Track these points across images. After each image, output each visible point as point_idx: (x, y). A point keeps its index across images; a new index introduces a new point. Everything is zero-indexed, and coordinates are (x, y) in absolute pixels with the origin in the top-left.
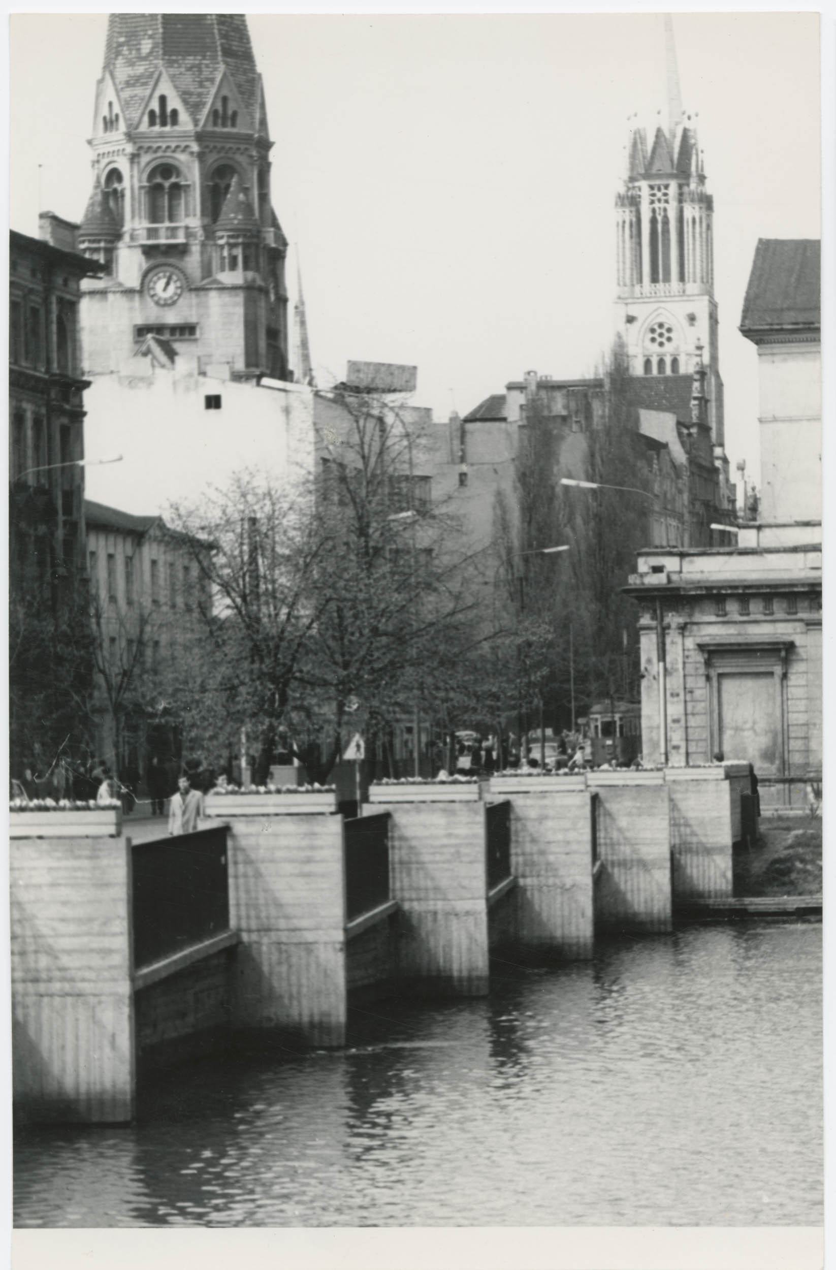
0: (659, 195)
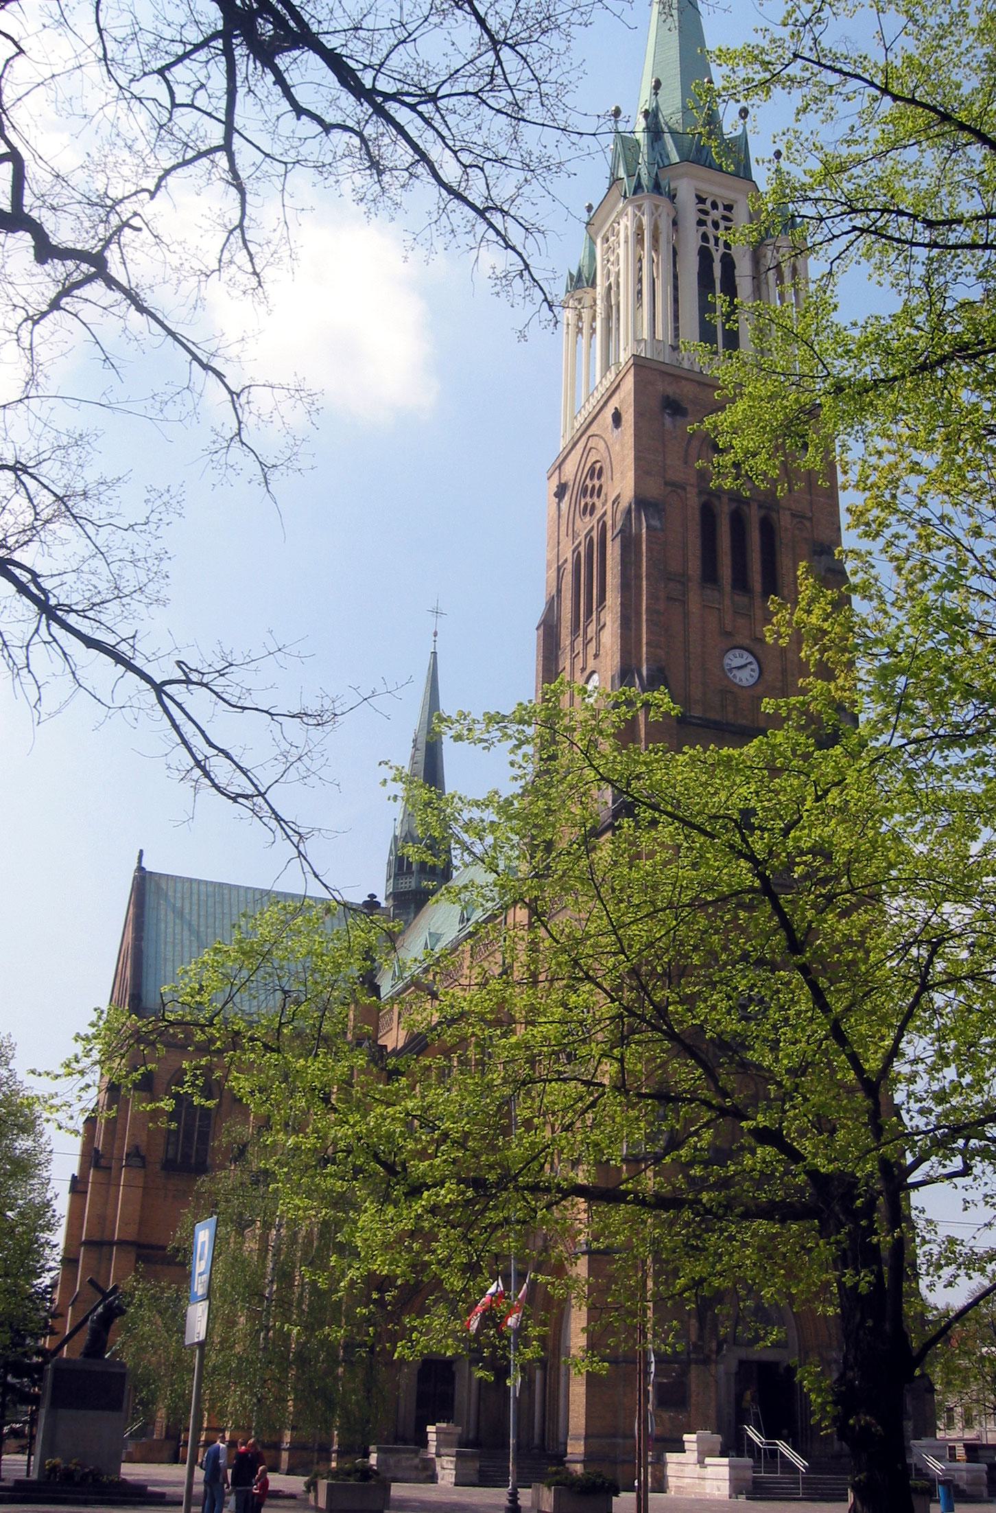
0: (716, 214)
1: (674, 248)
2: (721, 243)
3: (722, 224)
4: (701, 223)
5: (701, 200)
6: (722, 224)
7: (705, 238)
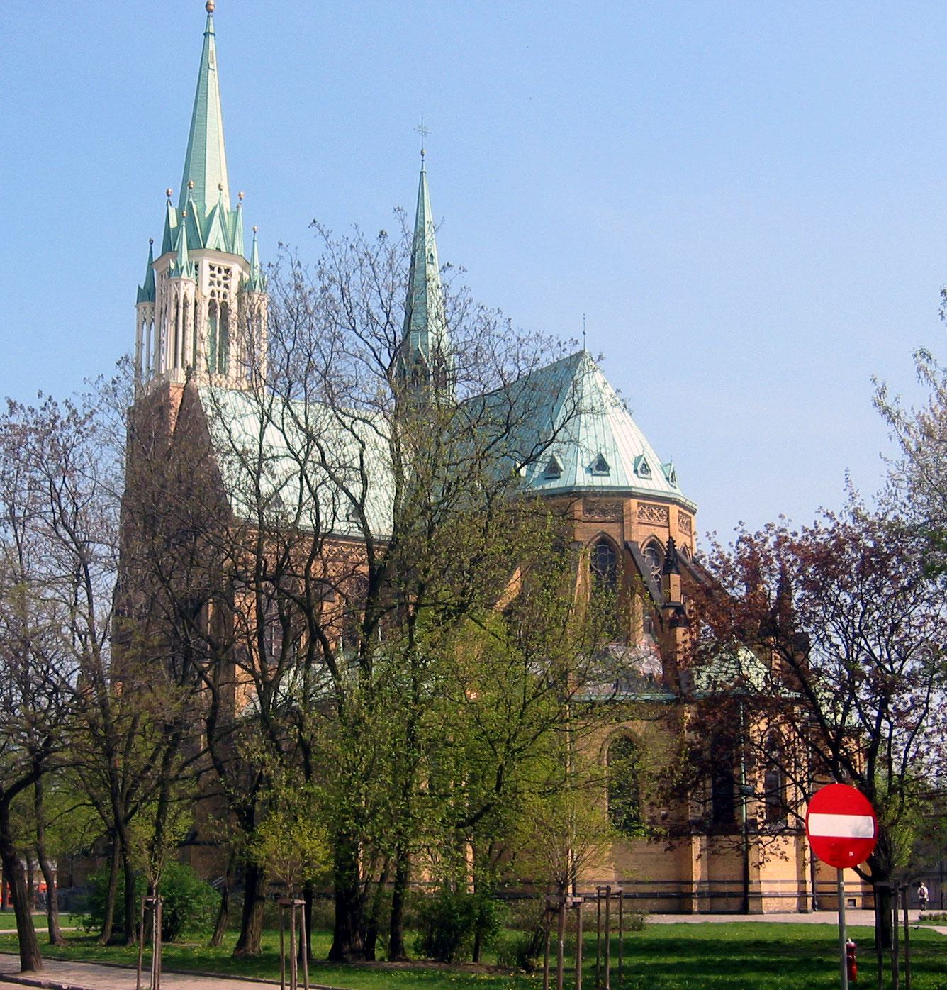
0: (220, 277)
2: (221, 294)
4: (212, 283)
5: (212, 268)
7: (213, 294)
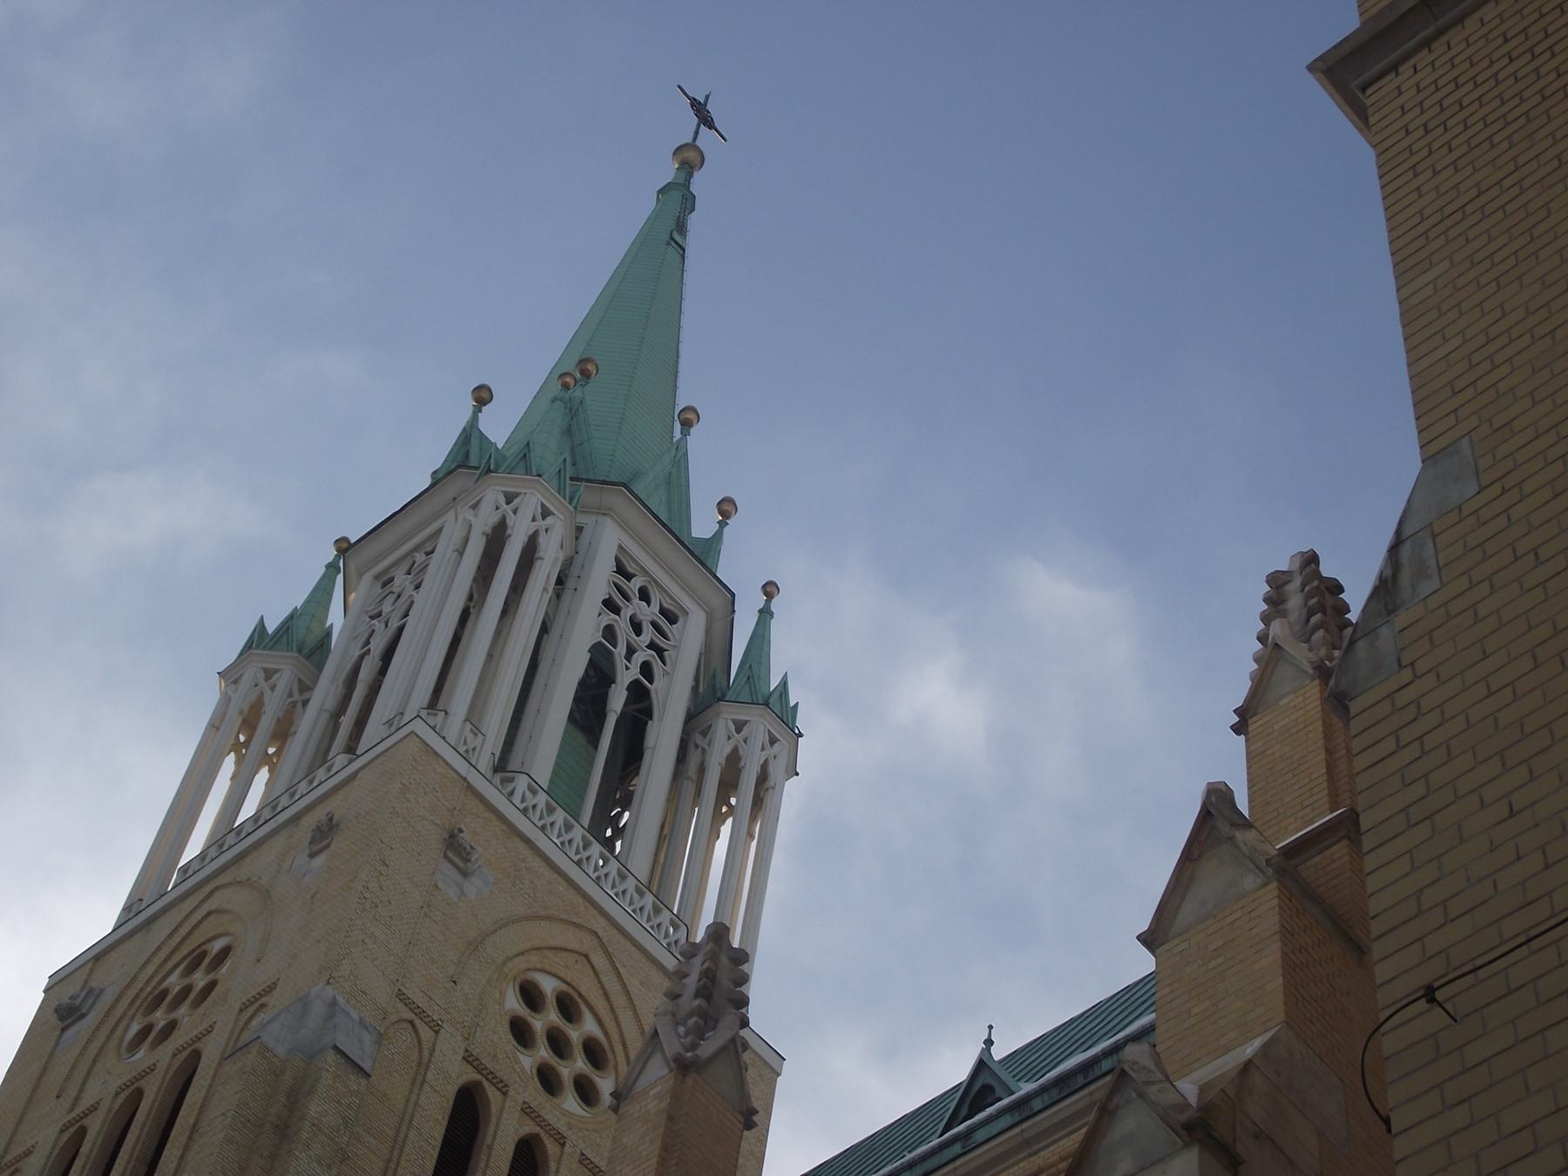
1: (544, 623)
3: (648, 634)
4: (609, 604)
6: (648, 634)
7: (609, 632)
